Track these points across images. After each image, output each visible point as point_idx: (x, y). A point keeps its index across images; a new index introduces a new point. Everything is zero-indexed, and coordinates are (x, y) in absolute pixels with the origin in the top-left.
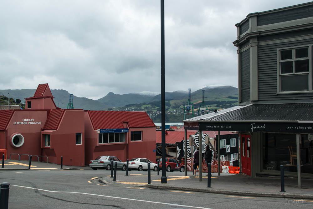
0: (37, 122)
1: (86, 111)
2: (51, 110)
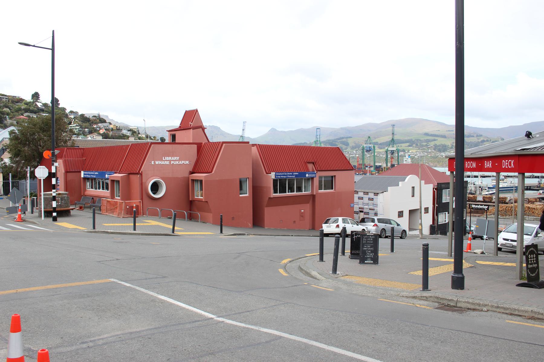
0: (183, 162)
1: (253, 145)
2: (204, 143)
